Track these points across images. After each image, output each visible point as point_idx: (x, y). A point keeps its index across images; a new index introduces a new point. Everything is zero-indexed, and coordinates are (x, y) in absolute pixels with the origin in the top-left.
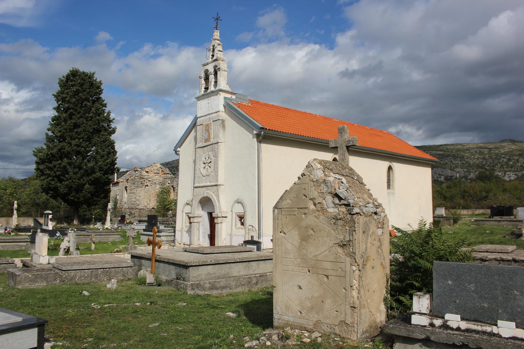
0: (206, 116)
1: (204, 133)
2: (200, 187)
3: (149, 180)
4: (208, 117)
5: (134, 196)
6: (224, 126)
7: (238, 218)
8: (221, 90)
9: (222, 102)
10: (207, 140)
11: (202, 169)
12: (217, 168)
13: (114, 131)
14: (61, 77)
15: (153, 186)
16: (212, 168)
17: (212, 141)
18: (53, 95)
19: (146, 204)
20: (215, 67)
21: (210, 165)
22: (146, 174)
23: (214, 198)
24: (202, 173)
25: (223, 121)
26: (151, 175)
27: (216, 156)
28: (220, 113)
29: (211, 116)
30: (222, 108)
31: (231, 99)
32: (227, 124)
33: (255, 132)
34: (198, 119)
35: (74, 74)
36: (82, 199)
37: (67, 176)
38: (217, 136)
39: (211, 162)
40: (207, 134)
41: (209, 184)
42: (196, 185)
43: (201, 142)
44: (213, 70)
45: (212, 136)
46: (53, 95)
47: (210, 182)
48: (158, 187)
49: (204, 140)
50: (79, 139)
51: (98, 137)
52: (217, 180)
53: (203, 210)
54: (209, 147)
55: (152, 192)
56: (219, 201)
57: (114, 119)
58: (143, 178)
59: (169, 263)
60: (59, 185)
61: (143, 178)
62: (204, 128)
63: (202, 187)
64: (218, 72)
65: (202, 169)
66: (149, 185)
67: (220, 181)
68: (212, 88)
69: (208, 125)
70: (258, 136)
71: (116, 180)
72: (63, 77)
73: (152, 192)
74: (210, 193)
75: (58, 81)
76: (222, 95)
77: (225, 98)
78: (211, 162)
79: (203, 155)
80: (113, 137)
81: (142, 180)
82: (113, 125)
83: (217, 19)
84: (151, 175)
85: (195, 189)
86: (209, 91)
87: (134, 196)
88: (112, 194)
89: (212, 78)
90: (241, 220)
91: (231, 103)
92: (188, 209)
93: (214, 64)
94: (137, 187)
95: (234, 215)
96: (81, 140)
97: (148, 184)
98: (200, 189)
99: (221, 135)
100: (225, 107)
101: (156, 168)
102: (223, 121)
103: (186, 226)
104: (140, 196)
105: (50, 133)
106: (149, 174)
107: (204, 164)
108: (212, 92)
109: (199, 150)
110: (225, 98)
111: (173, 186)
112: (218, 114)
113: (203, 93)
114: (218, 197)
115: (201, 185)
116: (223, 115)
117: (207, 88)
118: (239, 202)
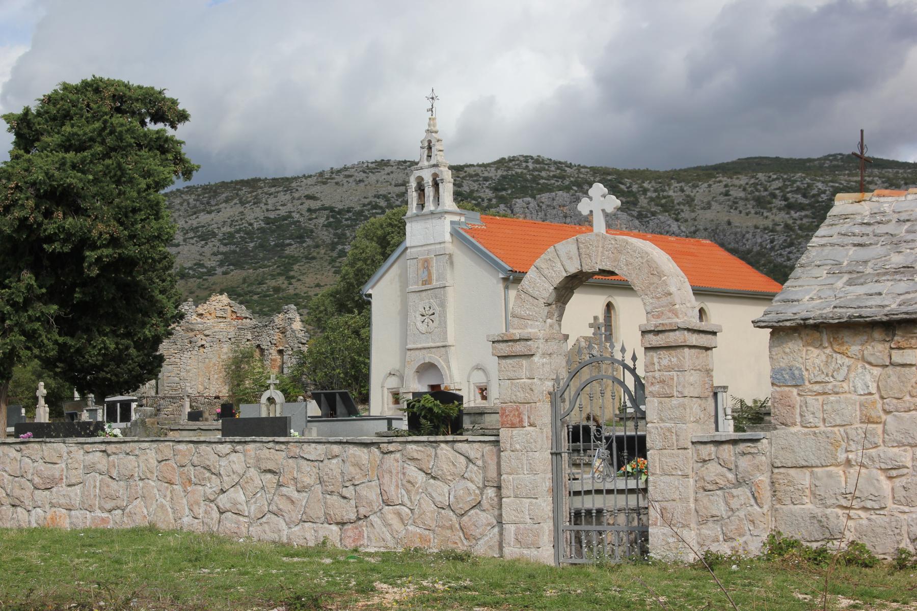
1: (420, 272)
2: (417, 349)
3: (207, 332)
4: (425, 248)
5: (176, 371)
6: (452, 263)
7: (477, 391)
8: (446, 212)
9: (448, 228)
10: (425, 283)
11: (419, 324)
12: (445, 323)
15: (216, 347)
16: (436, 323)
17: (435, 283)
19: (201, 388)
21: (432, 317)
22: (199, 320)
23: (441, 363)
24: (420, 329)
25: (450, 256)
26: (210, 321)
27: (443, 305)
28: (447, 245)
29: (429, 247)
30: (448, 237)
31: (459, 223)
32: (455, 259)
33: (501, 276)
34: (409, 250)
36: (126, 376)
38: (441, 277)
39: (433, 314)
40: (426, 273)
41: (433, 345)
42: (409, 346)
43: (417, 283)
44: (431, 179)
45: (434, 277)
47: (433, 341)
48: (226, 348)
49: (420, 282)
52: (445, 339)
53: (419, 382)
54: (429, 292)
55: (214, 361)
56: (449, 367)
58: (192, 330)
61: (192, 330)
62: (420, 265)
63: (420, 349)
64: (440, 185)
65: (419, 324)
66: (207, 345)
67: (451, 340)
68: (430, 206)
69: (426, 261)
70: (505, 280)
73: (214, 361)
74: (434, 357)
76: (449, 218)
77: (452, 223)
78: (433, 314)
79: (419, 304)
81: (191, 334)
83: (433, 98)
84: (210, 321)
85: (409, 352)
86: (425, 210)
87: (176, 371)
89: (429, 191)
90: (482, 393)
91: (461, 231)
92: (393, 383)
93: (433, 170)
94: (182, 350)
95: (472, 387)
97: (203, 342)
98: (417, 352)
99: (448, 276)
100: (452, 235)
101: (219, 306)
102: (450, 256)
103: (389, 409)
104: (188, 371)
105: (583, 344)
106: (205, 320)
107: (423, 316)
108: (432, 213)
109: (413, 297)
110: (452, 223)
111: (258, 346)
112: (442, 245)
113: (414, 211)
114: (447, 362)
115: (419, 346)
116: (450, 247)
117: (422, 206)
118: (478, 368)
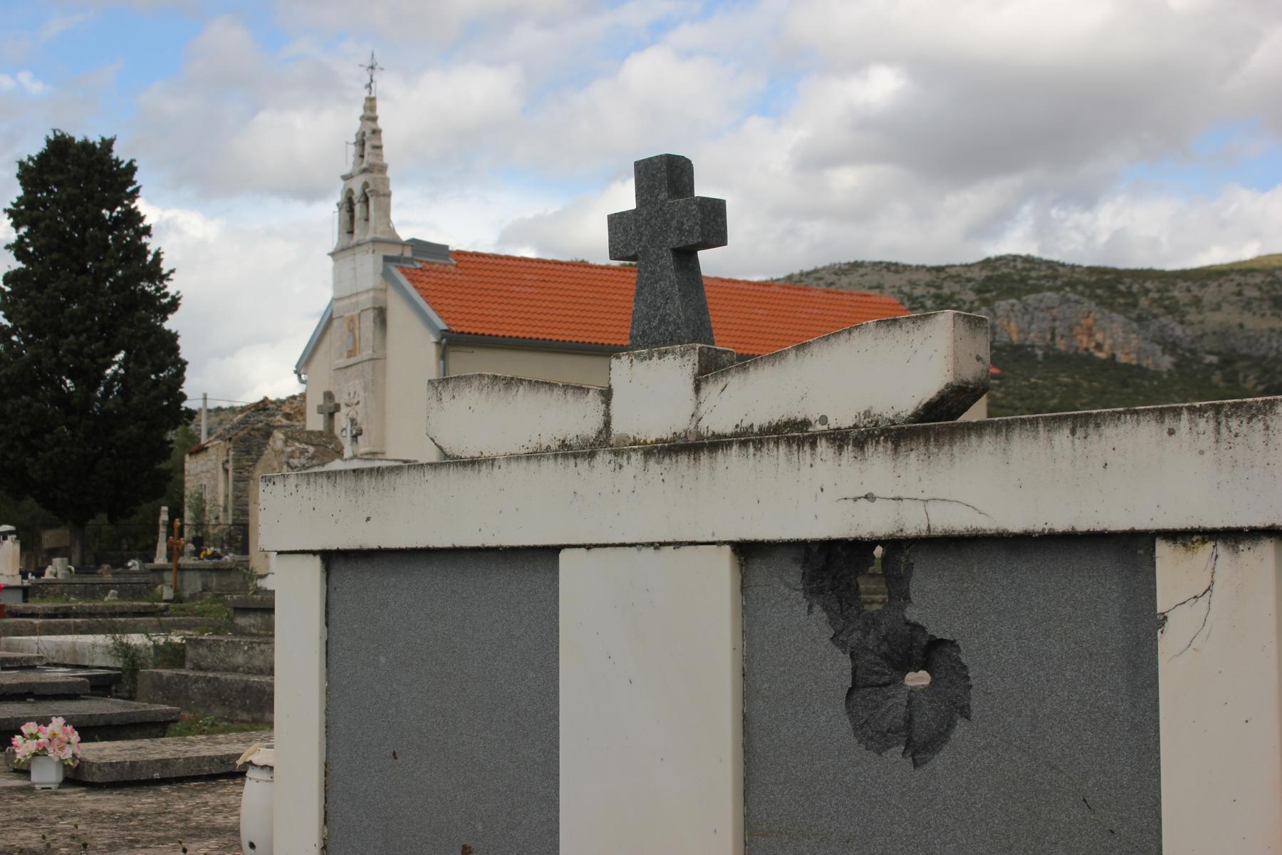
0: (350, 297)
13: (174, 305)
14: (25, 159)
18: (5, 211)
20: (366, 185)
22: (285, 422)
35: (60, 147)
37: (47, 436)
46: (5, 211)
49: (345, 354)
50: (78, 334)
51: (131, 325)
54: (354, 368)
57: (172, 271)
59: (193, 570)
60: (29, 460)
62: (345, 325)
69: (352, 320)
71: (203, 442)
72: (30, 158)
75: (16, 170)
80: (172, 323)
82: (171, 288)
83: (372, 68)
88: (190, 486)
96: (83, 337)
